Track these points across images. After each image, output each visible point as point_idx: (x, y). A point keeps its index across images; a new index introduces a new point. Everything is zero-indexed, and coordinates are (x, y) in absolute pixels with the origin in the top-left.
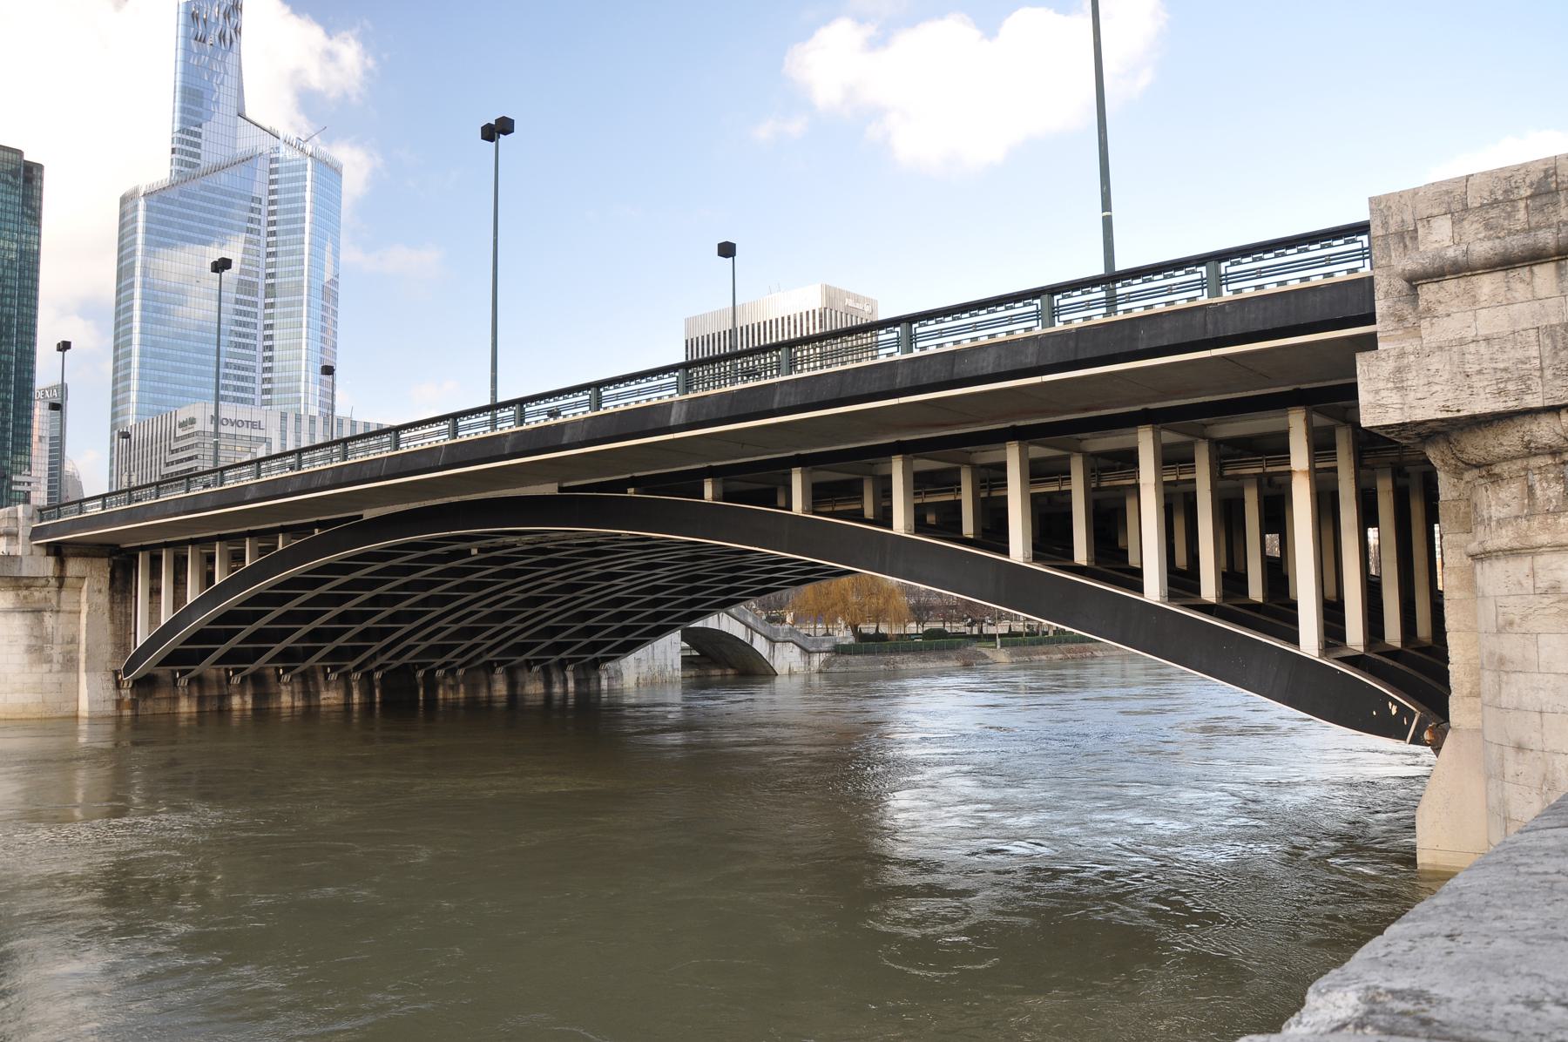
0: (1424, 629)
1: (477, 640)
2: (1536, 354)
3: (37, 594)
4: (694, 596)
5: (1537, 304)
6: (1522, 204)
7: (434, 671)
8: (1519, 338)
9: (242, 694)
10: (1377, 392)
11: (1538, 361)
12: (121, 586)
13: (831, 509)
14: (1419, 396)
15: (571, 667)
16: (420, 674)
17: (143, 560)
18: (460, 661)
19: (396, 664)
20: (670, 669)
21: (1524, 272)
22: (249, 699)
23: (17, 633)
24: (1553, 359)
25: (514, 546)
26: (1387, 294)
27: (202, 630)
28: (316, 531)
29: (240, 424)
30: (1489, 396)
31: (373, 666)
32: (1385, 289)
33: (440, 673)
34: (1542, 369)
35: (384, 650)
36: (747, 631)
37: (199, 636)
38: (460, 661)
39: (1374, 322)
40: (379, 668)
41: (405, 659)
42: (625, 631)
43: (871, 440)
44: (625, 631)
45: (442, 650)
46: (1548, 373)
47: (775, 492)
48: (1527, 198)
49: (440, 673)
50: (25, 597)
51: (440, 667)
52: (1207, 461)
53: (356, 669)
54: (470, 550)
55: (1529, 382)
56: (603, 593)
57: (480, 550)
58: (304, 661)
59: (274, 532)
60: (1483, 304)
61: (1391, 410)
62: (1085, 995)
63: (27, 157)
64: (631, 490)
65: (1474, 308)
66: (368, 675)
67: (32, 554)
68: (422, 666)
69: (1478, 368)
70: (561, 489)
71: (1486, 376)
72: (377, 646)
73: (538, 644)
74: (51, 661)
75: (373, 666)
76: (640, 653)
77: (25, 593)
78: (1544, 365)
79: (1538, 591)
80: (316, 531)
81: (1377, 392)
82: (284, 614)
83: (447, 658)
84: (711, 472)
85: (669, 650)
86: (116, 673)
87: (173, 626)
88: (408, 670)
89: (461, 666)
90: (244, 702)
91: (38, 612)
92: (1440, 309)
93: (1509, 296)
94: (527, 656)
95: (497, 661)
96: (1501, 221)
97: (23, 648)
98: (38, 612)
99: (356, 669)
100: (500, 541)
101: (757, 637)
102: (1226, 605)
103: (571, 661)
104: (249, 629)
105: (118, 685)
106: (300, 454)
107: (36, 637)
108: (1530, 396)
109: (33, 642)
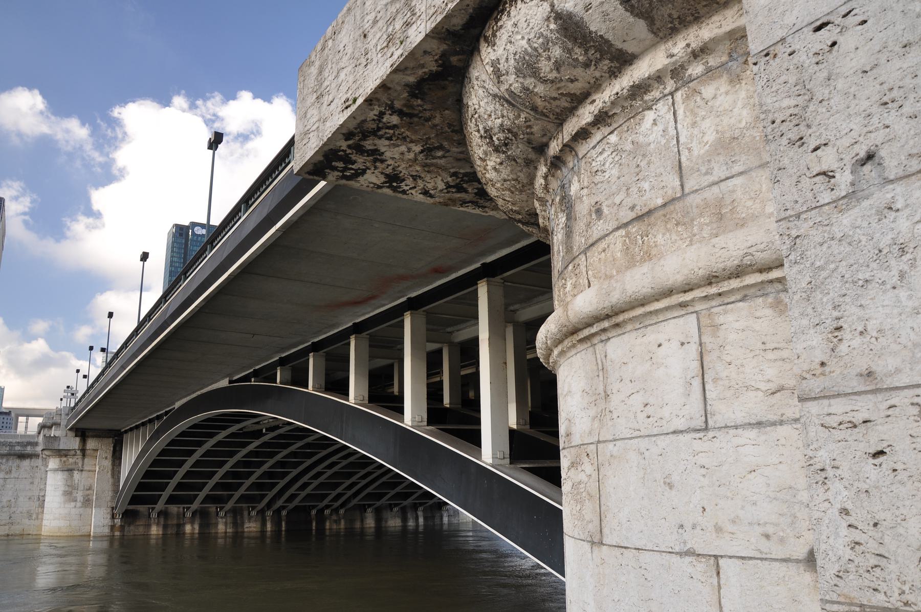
3: (70, 460)
9: (192, 523)
16: (314, 512)
22: (197, 527)
23: (59, 483)
49: (327, 512)
50: (64, 462)
67: (66, 436)
74: (76, 501)
77: (64, 459)
91: (70, 470)
97: (61, 492)
98: (70, 470)
107: (69, 486)
109: (67, 489)
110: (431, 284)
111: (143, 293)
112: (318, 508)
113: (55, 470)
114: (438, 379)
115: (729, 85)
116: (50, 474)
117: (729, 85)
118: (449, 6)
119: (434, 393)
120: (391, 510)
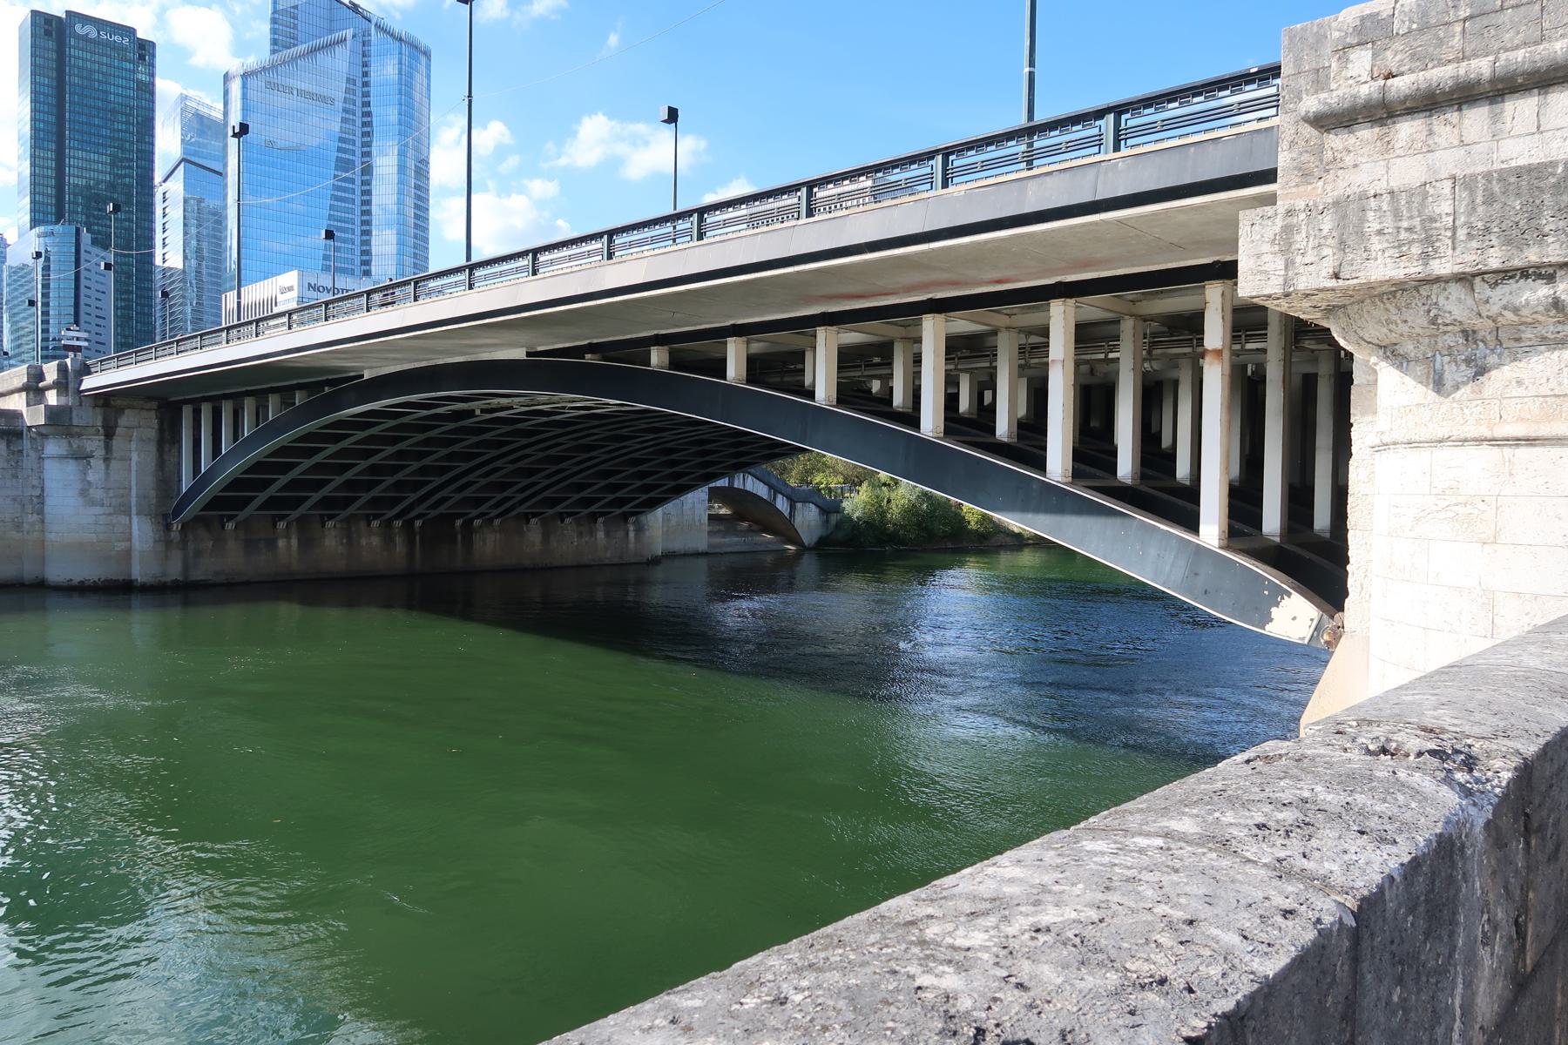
0: (1322, 519)
1: (507, 493)
2: (1449, 210)
4: (736, 461)
5: (1462, 151)
6: (1458, 28)
7: (472, 520)
8: (1431, 191)
9: (288, 537)
10: (1258, 256)
11: (1451, 219)
12: (168, 437)
13: (778, 379)
14: (1307, 260)
15: (601, 520)
16: (459, 522)
17: (187, 412)
18: (495, 512)
19: (433, 513)
20: (698, 524)
21: (1453, 116)
22: (294, 542)
23: (72, 477)
24: (1470, 215)
25: (511, 408)
26: (1292, 143)
27: (236, 479)
28: (326, 388)
29: (321, 289)
30: (1388, 260)
31: (413, 514)
32: (1291, 139)
33: (477, 522)
34: (1454, 229)
35: (421, 500)
36: (769, 492)
37: (235, 484)
38: (495, 512)
39: (1275, 181)
40: (418, 517)
41: (442, 509)
42: (647, 488)
43: (791, 311)
44: (647, 488)
45: (478, 502)
46: (1462, 234)
47: (757, 367)
48: (1465, 20)
49: (477, 522)
51: (477, 517)
52: (1131, 346)
53: (397, 516)
54: (474, 411)
55: (1437, 244)
56: (616, 454)
57: (483, 411)
58: (345, 509)
59: (293, 389)
60: (1399, 152)
61: (1273, 277)
62: (1149, 728)
63: (140, 35)
64: (588, 356)
65: (1386, 156)
66: (409, 525)
67: (81, 405)
68: (459, 516)
69: (1379, 227)
70: (528, 354)
71: (1387, 237)
72: (413, 497)
73: (568, 498)
75: (413, 514)
76: (670, 507)
78: (1458, 223)
79: (1434, 491)
80: (326, 388)
81: (1258, 256)
82: (312, 467)
83: (482, 509)
84: (659, 340)
85: (696, 504)
86: (165, 516)
87: (212, 472)
88: (451, 518)
89: (498, 516)
90: (289, 545)
92: (1347, 159)
93: (1430, 142)
94: (559, 509)
95: (567, 513)
96: (1431, 49)
99: (397, 516)
100: (495, 401)
101: (780, 497)
102: (1143, 488)
103: (602, 514)
104: (284, 479)
105: (168, 527)
106: (290, 315)
108: (1438, 261)
110: (942, 249)
111: (473, 197)
112: (238, 518)
113: (61, 458)
114: (888, 371)
115: (1431, 79)
116: (48, 464)
117: (1431, 79)
118: (1480, 266)
119: (951, 401)
120: (562, 521)
